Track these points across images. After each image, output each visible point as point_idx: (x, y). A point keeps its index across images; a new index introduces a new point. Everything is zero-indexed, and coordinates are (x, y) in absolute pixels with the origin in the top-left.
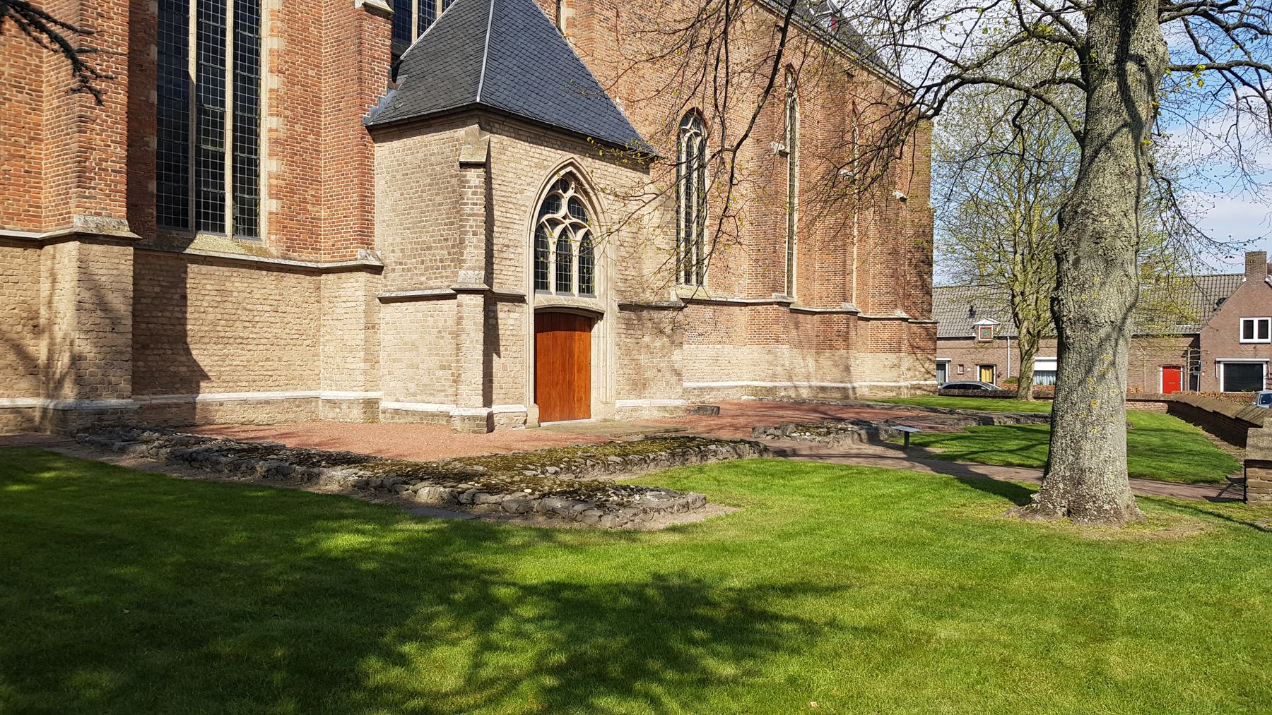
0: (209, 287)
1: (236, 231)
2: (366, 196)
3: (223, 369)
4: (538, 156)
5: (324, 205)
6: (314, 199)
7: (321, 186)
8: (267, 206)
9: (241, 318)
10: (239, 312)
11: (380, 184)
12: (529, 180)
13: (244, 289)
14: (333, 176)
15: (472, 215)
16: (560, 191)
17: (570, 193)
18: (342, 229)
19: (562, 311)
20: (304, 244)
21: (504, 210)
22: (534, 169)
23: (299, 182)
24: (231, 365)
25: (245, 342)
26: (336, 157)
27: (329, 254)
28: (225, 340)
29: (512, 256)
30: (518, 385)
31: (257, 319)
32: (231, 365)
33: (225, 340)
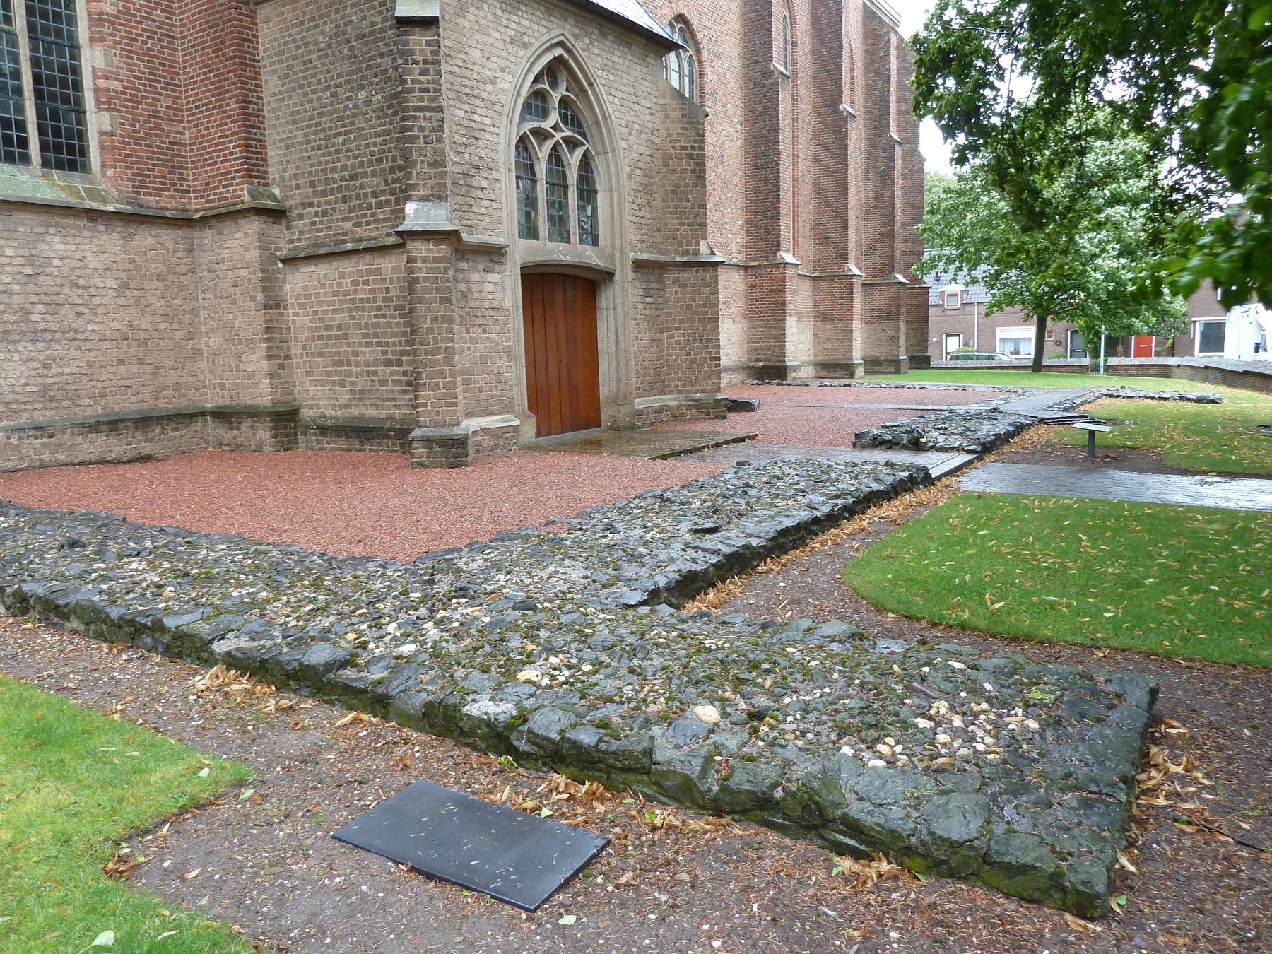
0: (9, 252)
1: (45, 163)
2: (250, 102)
3: (48, 381)
4: (514, 26)
5: (189, 122)
6: (172, 112)
7: (181, 92)
8: (97, 122)
9: (70, 300)
10: (66, 290)
11: (270, 84)
12: (503, 63)
13: (69, 253)
14: (198, 75)
15: (420, 109)
16: (547, 87)
17: (562, 91)
18: (218, 157)
19: (559, 270)
20: (162, 183)
21: (467, 107)
22: (510, 47)
23: (145, 85)
24: (62, 374)
25: (79, 336)
26: (199, 45)
27: (202, 197)
28: (48, 336)
29: (484, 184)
30: (504, 386)
31: (96, 300)
32: (62, 374)
33: (48, 336)
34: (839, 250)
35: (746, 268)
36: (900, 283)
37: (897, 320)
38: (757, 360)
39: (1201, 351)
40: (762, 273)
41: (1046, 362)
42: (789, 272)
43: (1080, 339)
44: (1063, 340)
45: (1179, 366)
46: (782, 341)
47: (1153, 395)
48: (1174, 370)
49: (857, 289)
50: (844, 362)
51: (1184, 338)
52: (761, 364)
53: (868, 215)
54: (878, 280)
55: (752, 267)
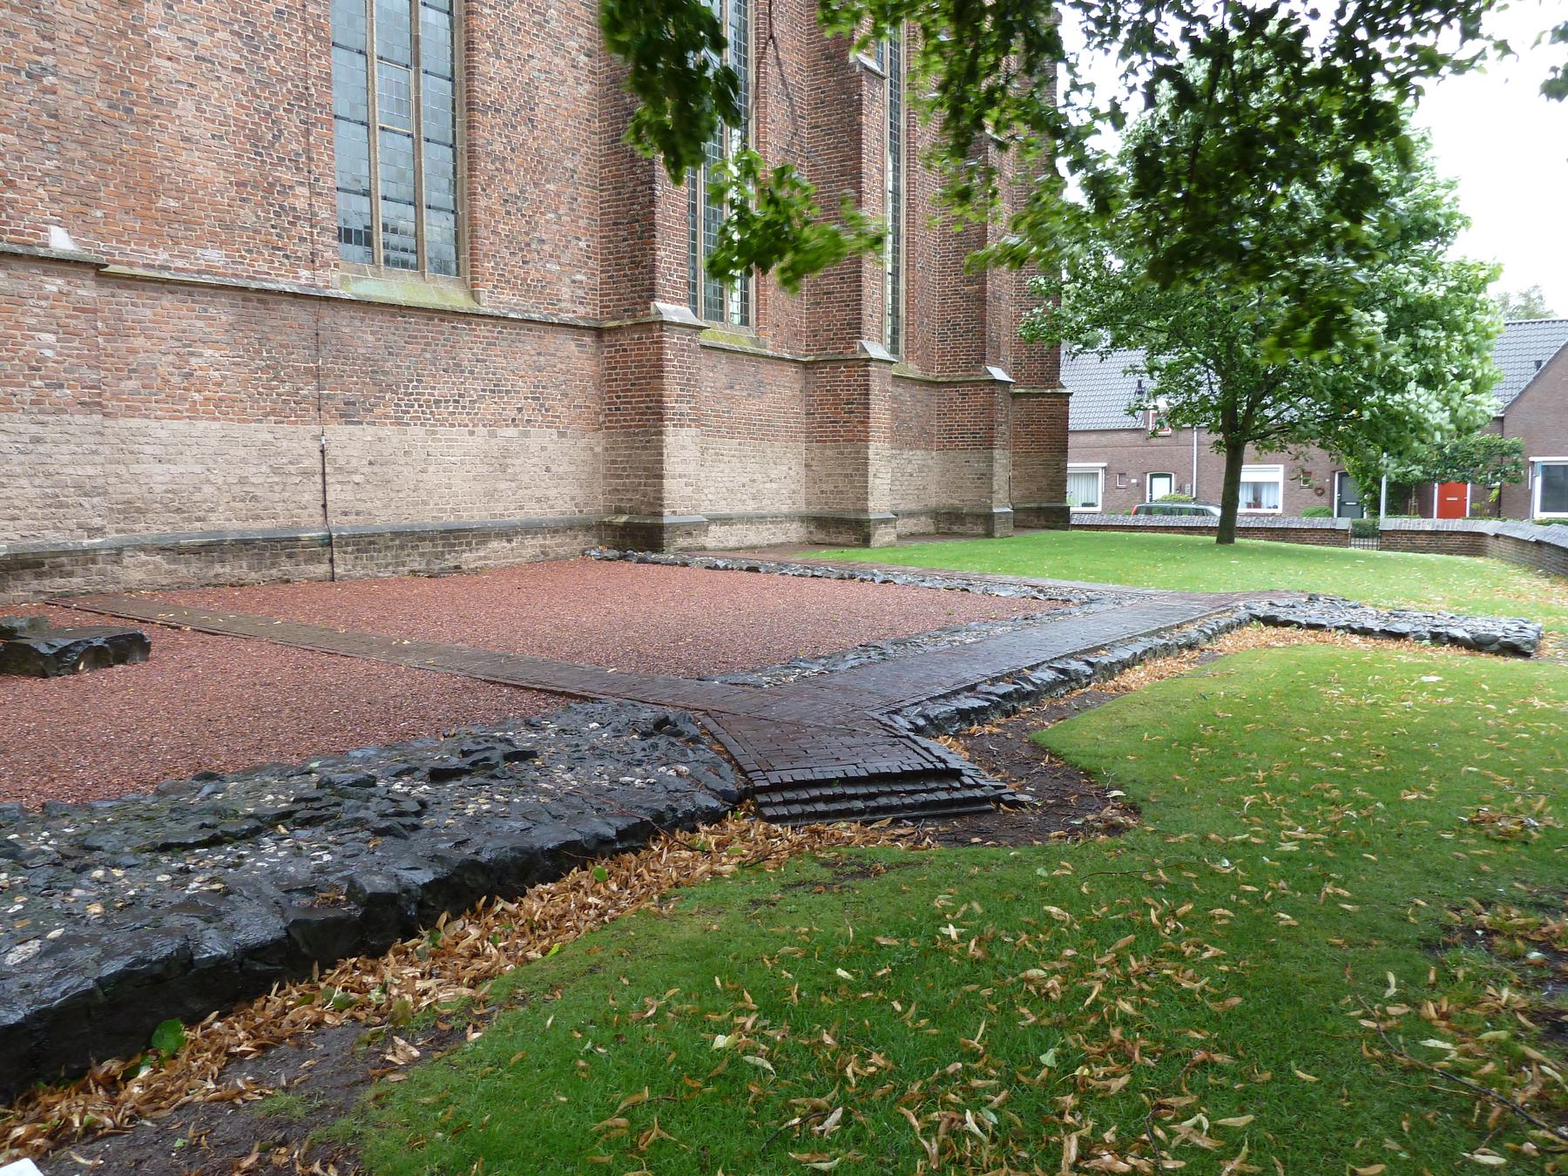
34: (847, 315)
35: (599, 332)
36: (994, 381)
37: (988, 444)
38: (619, 511)
39: (1544, 509)
40: (625, 341)
41: (1241, 522)
42: (672, 339)
43: (1352, 486)
44: (1327, 487)
45: (1497, 536)
46: (655, 474)
47: (1369, 624)
48: (1490, 542)
49: (878, 385)
50: (853, 516)
51: (1516, 488)
52: (623, 519)
53: (944, 265)
54: (959, 376)
55: (610, 330)
